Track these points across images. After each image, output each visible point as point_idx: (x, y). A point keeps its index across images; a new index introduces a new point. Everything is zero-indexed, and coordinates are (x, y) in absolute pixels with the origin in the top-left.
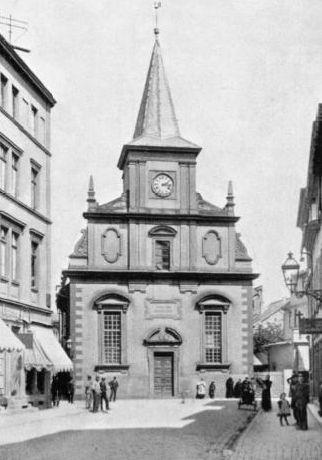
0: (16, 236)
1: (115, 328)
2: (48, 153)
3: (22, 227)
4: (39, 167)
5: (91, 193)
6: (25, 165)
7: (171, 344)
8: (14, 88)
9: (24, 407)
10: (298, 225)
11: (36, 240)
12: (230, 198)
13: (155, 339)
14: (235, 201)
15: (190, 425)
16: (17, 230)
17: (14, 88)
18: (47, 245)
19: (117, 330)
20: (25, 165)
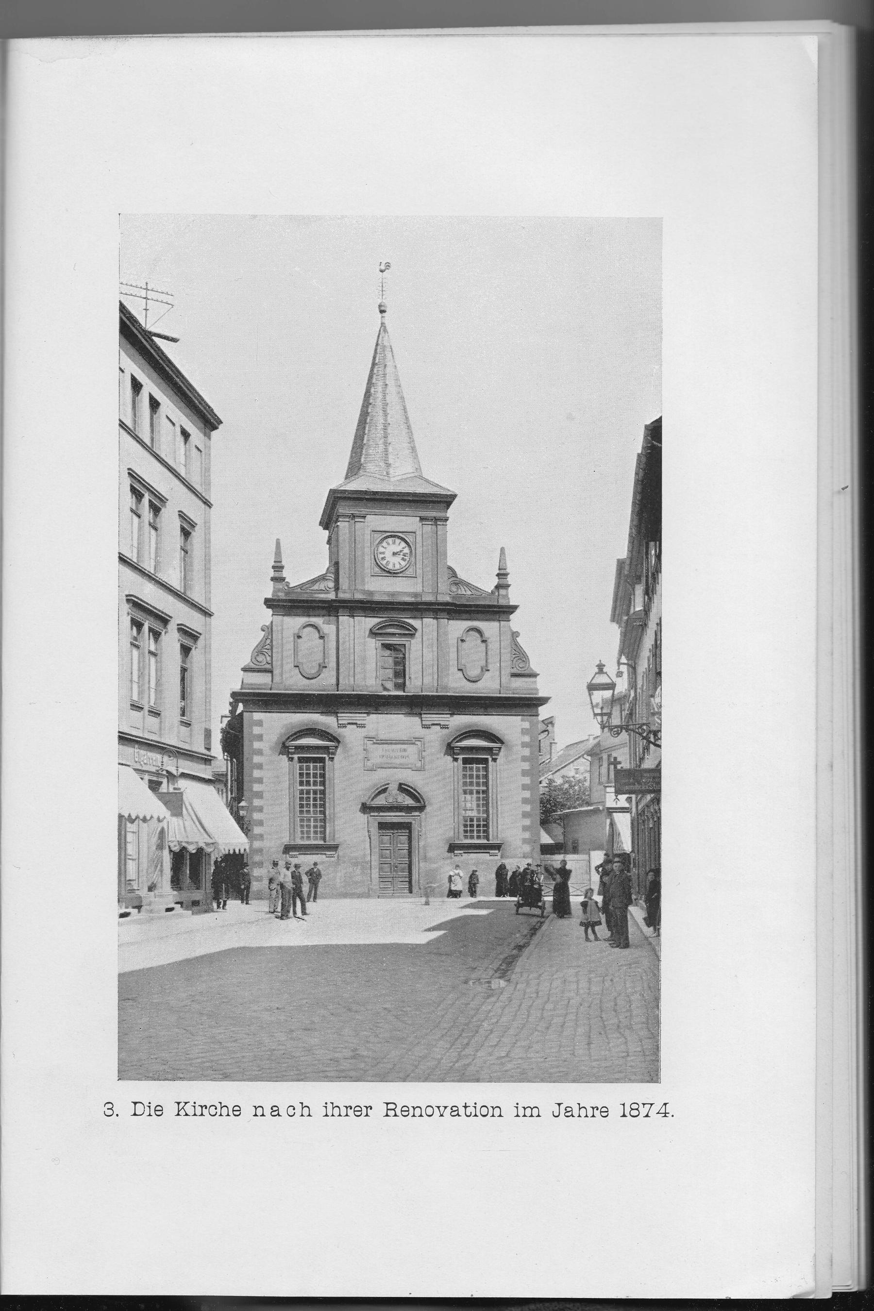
2: (207, 503)
3: (164, 620)
5: (278, 567)
12: (502, 575)
14: (510, 580)
16: (157, 626)
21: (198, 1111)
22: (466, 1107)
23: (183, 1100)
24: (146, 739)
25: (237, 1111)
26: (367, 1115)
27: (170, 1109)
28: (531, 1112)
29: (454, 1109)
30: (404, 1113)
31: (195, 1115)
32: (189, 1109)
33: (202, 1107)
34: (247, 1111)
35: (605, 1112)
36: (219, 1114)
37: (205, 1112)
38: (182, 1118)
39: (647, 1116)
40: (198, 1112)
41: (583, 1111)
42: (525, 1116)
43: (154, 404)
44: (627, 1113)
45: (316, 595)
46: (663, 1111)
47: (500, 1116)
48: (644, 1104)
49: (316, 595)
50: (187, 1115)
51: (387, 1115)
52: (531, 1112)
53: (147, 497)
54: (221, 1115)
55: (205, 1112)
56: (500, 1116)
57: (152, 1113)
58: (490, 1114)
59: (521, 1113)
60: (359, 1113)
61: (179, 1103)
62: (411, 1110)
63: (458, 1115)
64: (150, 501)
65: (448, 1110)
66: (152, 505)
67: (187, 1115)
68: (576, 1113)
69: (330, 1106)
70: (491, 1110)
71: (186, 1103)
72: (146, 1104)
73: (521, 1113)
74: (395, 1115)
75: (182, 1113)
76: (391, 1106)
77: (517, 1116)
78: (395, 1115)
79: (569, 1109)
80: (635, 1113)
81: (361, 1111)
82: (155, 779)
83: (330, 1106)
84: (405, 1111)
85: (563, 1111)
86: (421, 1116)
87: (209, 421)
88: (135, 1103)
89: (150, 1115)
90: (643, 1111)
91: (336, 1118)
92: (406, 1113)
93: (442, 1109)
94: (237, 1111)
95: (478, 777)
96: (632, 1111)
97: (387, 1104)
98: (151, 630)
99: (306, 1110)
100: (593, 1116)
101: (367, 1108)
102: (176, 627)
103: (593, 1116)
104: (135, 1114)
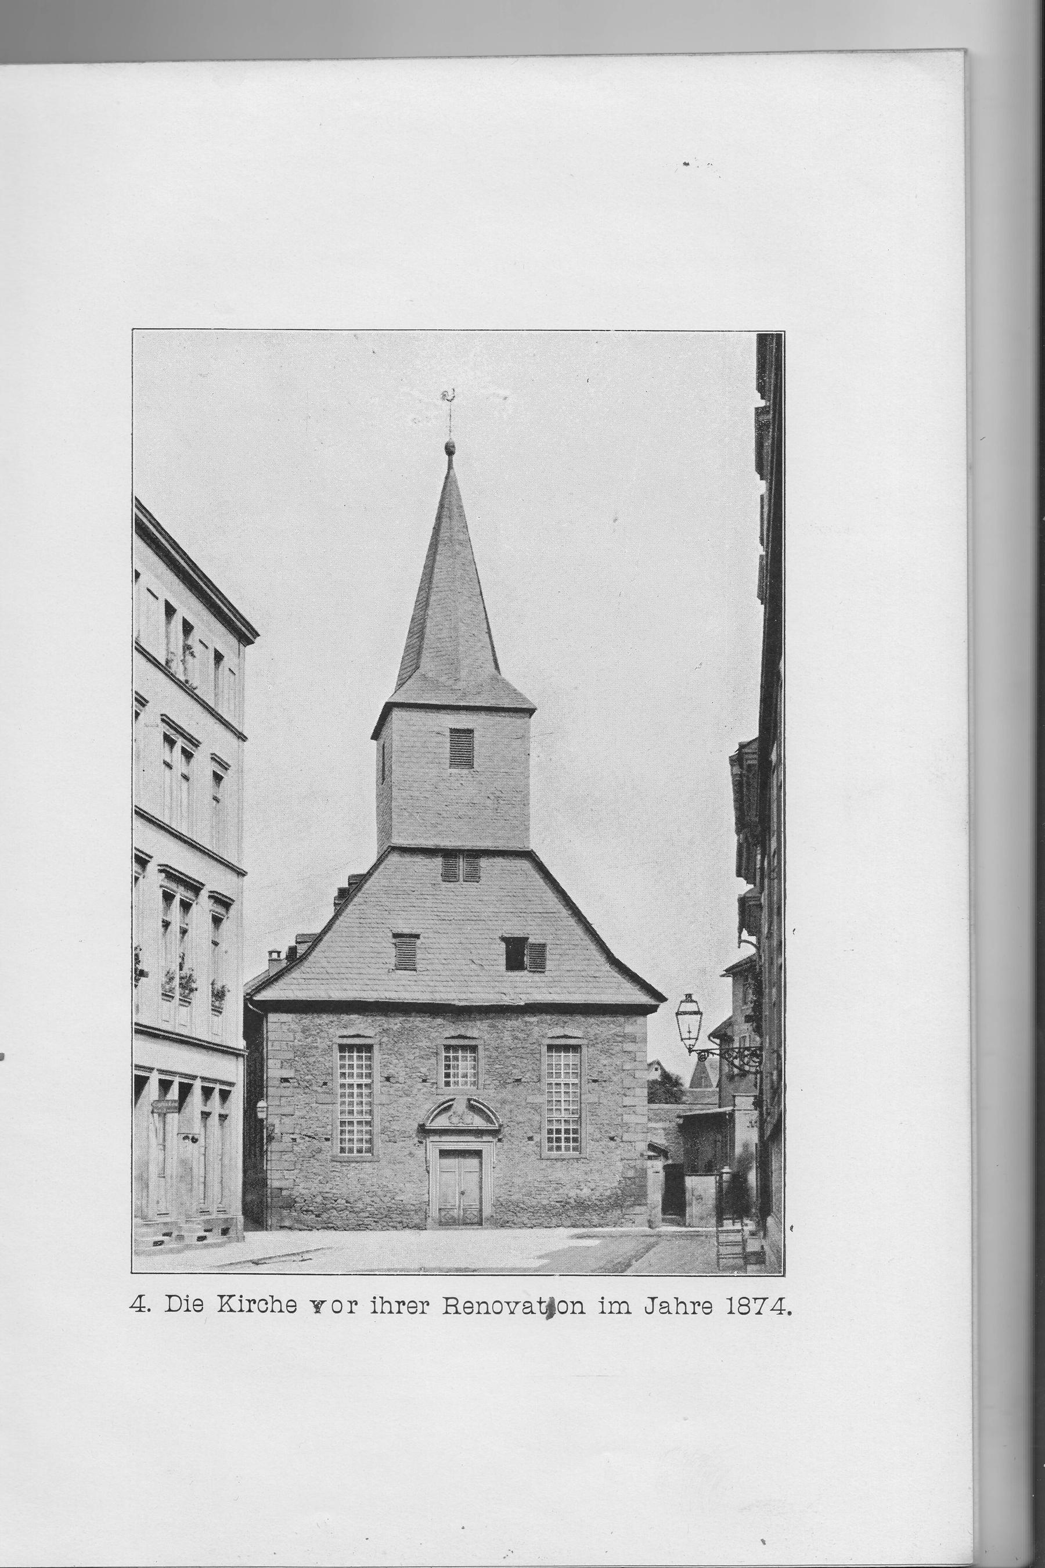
0: (186, 906)
1: (360, 1076)
2: (242, 737)
3: (195, 888)
4: (225, 767)
6: (202, 766)
7: (479, 1133)
8: (185, 623)
9: (201, 1239)
10: (739, 875)
11: (220, 910)
13: (442, 1122)
15: (733, 1147)
16: (190, 895)
17: (185, 623)
18: (240, 925)
19: (365, 1081)
20: (202, 766)
22: (540, 1303)
24: (177, 1034)
25: (292, 1307)
26: (423, 1312)
27: (212, 1303)
28: (621, 1307)
29: (527, 1305)
30: (468, 1310)
31: (241, 1311)
32: (234, 1303)
33: (249, 1301)
34: (721, 1307)
35: (708, 1307)
36: (270, 1309)
37: (254, 1307)
39: (759, 1313)
40: (246, 1307)
41: (387, 1307)
43: (187, 628)
44: (735, 1310)
46: (778, 1307)
48: (755, 1299)
50: (231, 1310)
51: (447, 1312)
52: (621, 1307)
53: (180, 742)
55: (254, 1307)
56: (582, 1312)
57: (191, 1308)
58: (570, 1310)
60: (413, 1310)
62: (476, 1306)
64: (183, 748)
65: (520, 1306)
66: (184, 751)
67: (231, 1310)
68: (673, 1309)
69: (378, 1301)
70: (570, 1305)
71: (230, 1297)
72: (183, 1297)
73: (607, 1309)
74: (457, 1312)
75: (226, 1308)
76: (452, 1302)
77: (375, 1312)
78: (457, 1312)
80: (744, 1309)
81: (415, 1307)
82: (186, 1081)
83: (378, 1301)
84: (469, 1308)
85: (657, 1307)
86: (487, 1313)
87: (244, 633)
88: (170, 1297)
89: (188, 1310)
90: (755, 1307)
91: (387, 1316)
92: (470, 1310)
93: (512, 1305)
94: (292, 1307)
95: (351, 1140)
96: (743, 1306)
97: (447, 1299)
98: (182, 902)
100: (250, 1311)
102: (208, 894)
103: (694, 1313)
104: (170, 1310)
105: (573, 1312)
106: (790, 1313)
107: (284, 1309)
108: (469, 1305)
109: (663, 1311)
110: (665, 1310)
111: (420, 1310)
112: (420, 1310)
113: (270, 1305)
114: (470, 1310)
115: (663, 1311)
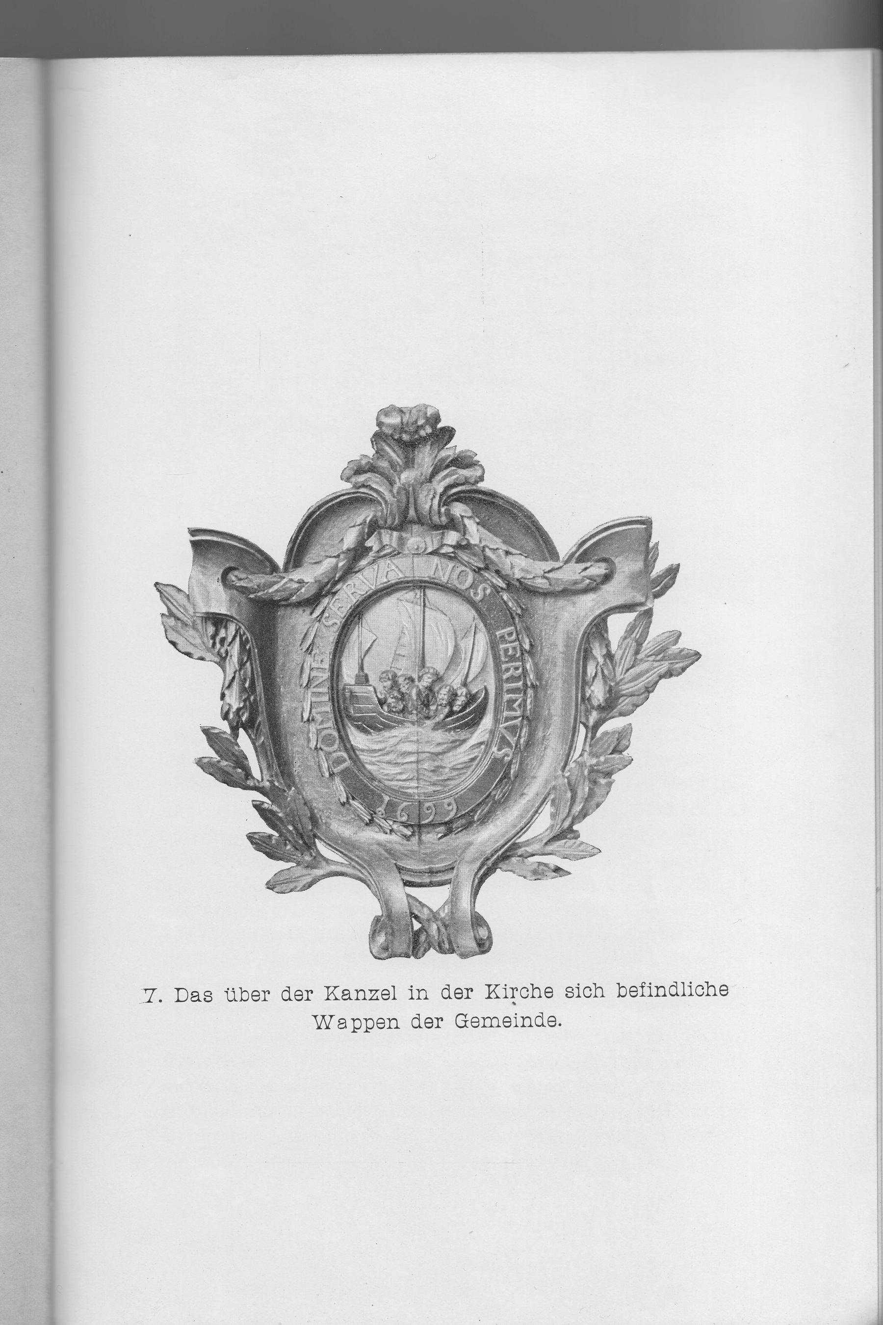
21: (509, 993)
23: (332, 984)
32: (500, 991)
36: (530, 995)
38: (493, 1001)
40: (654, 993)
41: (536, 992)
42: (658, 995)
45: (345, 862)
47: (426, 998)
49: (345, 862)
50: (497, 997)
54: (708, 995)
56: (397, 1027)
59: (415, 996)
61: (489, 986)
63: (199, 1000)
67: (497, 997)
73: (415, 996)
79: (346, 992)
86: (531, 1026)
88: (178, 989)
99: (599, 991)
101: (467, 990)
104: (178, 1001)
105: (390, 1028)
106: (560, 1025)
107: (501, 1024)
108: (459, 991)
109: (345, 997)
110: (196, 999)
111: (435, 1025)
112: (465, 995)
113: (705, 990)
114: (430, 1025)
115: (345, 997)
